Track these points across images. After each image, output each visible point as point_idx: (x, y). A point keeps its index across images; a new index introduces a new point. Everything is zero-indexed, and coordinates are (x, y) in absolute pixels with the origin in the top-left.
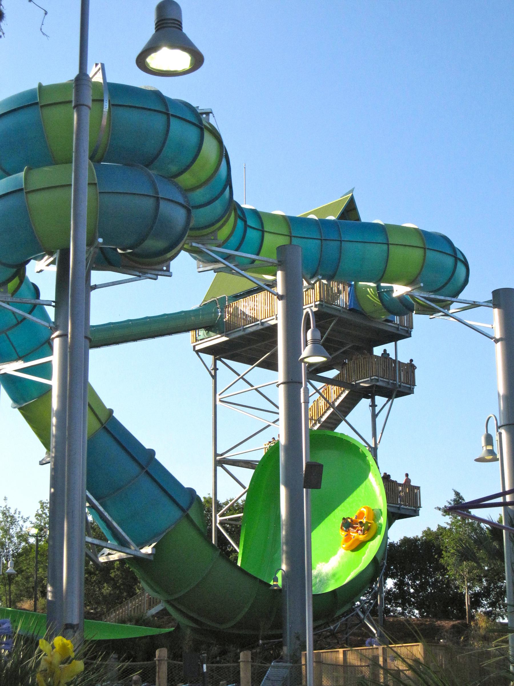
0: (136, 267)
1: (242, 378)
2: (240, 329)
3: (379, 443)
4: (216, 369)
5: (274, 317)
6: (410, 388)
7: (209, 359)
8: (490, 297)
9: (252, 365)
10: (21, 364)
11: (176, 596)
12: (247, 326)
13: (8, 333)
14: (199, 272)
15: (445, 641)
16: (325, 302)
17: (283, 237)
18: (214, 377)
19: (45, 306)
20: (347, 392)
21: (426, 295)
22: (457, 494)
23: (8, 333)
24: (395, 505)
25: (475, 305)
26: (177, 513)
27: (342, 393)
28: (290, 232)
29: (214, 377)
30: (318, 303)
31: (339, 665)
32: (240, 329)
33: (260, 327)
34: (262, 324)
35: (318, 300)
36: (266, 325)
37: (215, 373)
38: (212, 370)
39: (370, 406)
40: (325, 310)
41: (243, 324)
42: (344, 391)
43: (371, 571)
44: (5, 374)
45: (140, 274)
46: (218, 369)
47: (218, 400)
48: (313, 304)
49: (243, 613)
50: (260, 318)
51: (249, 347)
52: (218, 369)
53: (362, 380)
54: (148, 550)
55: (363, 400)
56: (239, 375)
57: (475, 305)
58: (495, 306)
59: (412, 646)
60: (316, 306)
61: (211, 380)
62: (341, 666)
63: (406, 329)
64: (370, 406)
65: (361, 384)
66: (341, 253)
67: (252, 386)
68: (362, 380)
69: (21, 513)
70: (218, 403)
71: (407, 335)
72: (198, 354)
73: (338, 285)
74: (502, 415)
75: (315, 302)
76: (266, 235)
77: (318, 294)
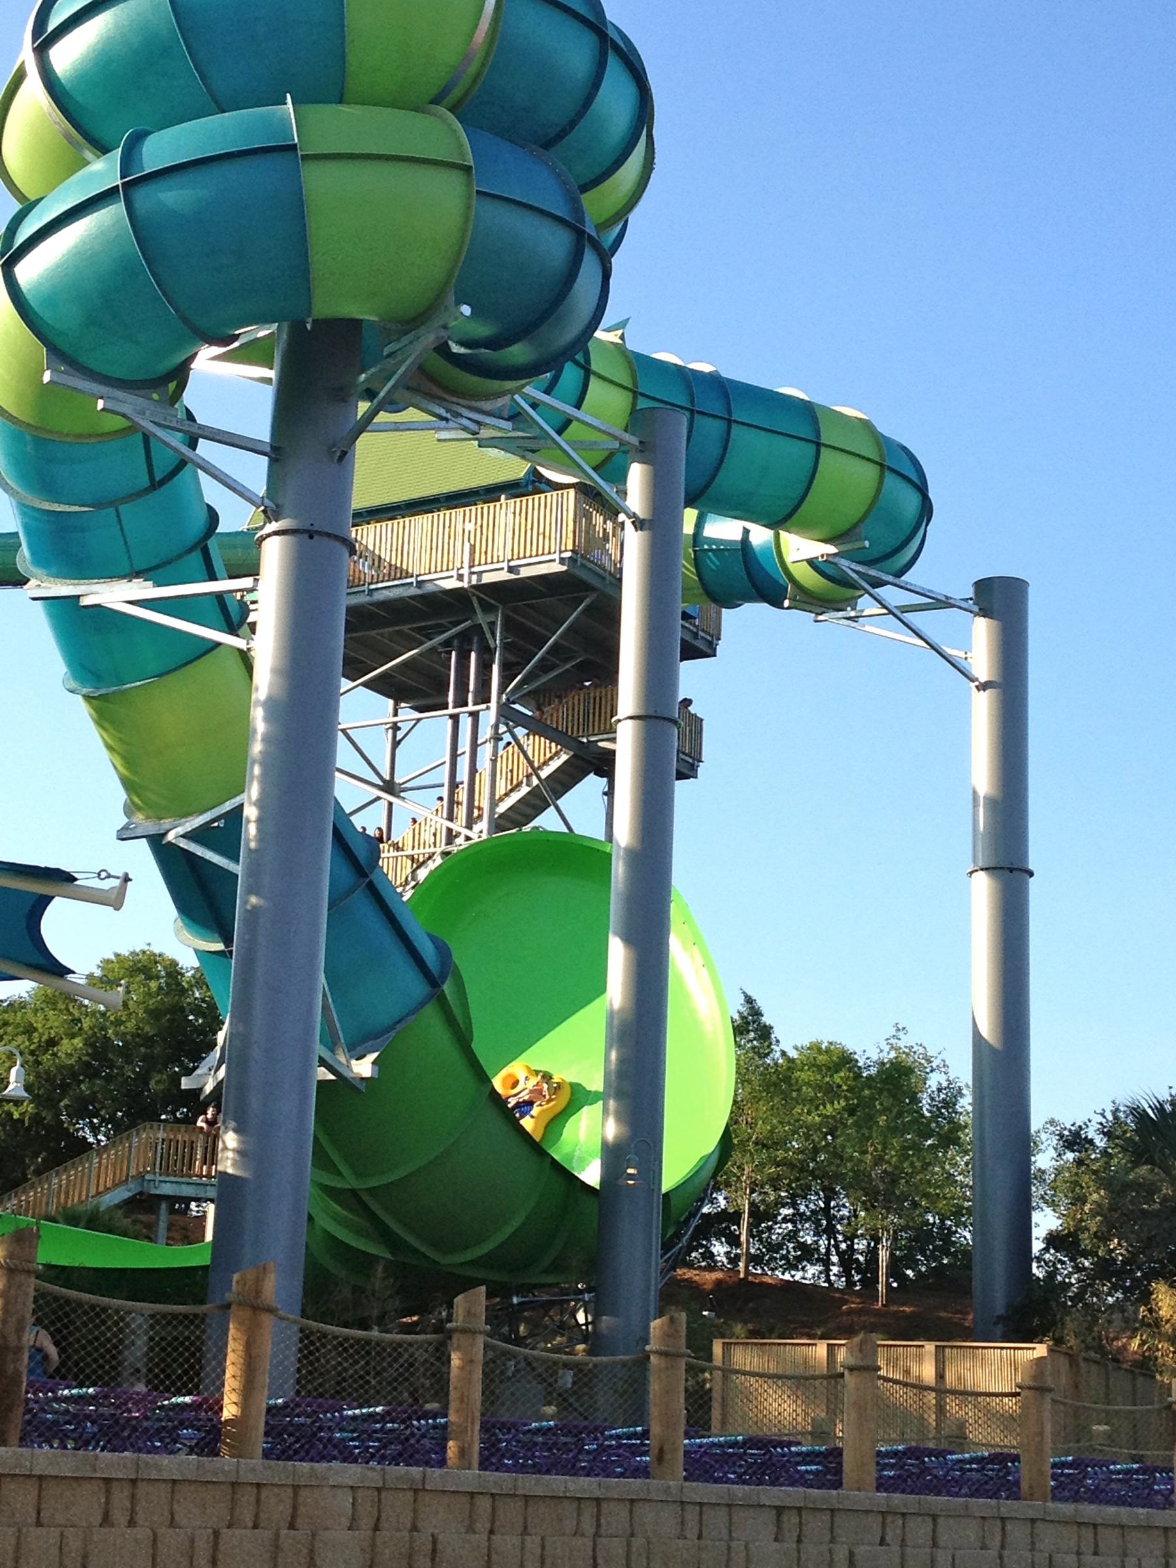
0: (445, 400)
2: (362, 588)
5: (454, 573)
6: (693, 765)
8: (970, 592)
10: (144, 589)
11: (373, 1183)
12: (380, 585)
13: (121, 508)
14: (439, 440)
15: (713, 1314)
16: (582, 556)
17: (622, 391)
20: (564, 757)
21: (860, 568)
22: (749, 1000)
23: (121, 508)
25: (943, 603)
26: (417, 987)
27: (551, 758)
28: (635, 383)
30: (569, 554)
31: (815, 1378)
32: (362, 588)
33: (413, 591)
34: (420, 584)
35: (570, 547)
36: (429, 588)
39: (605, 794)
40: (584, 575)
41: (368, 580)
42: (557, 754)
43: (715, 1157)
44: (98, 606)
45: (449, 416)
48: (556, 556)
49: (508, 1230)
50: (415, 573)
51: (397, 628)
53: (605, 736)
54: (363, 1068)
55: (592, 776)
57: (943, 603)
58: (984, 612)
59: (1015, 1348)
60: (562, 561)
62: (823, 1377)
63: (709, 638)
64: (605, 794)
65: (601, 744)
66: (725, 449)
68: (605, 736)
71: (709, 651)
73: (605, 522)
74: (980, 843)
75: (561, 552)
76: (594, 383)
77: (571, 535)
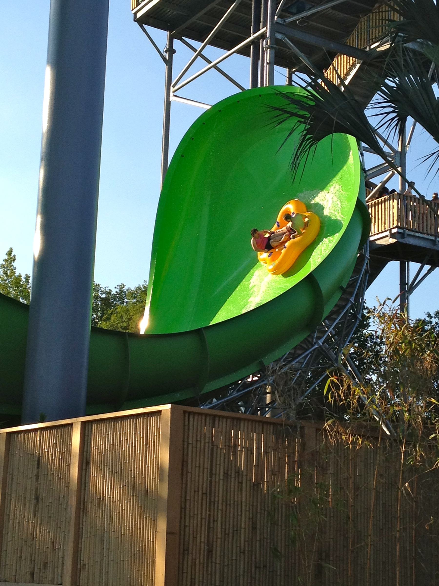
1: (215, 66)
3: (409, 144)
4: (171, 51)
7: (161, 36)
9: (229, 50)
18: (169, 63)
19: (370, 180)
24: (425, 236)
29: (169, 63)
37: (171, 57)
38: (166, 52)
46: (174, 52)
47: (171, 94)
52: (174, 52)
56: (210, 62)
61: (164, 67)
67: (210, 62)
69: (332, 197)
70: (172, 98)
72: (142, 27)
